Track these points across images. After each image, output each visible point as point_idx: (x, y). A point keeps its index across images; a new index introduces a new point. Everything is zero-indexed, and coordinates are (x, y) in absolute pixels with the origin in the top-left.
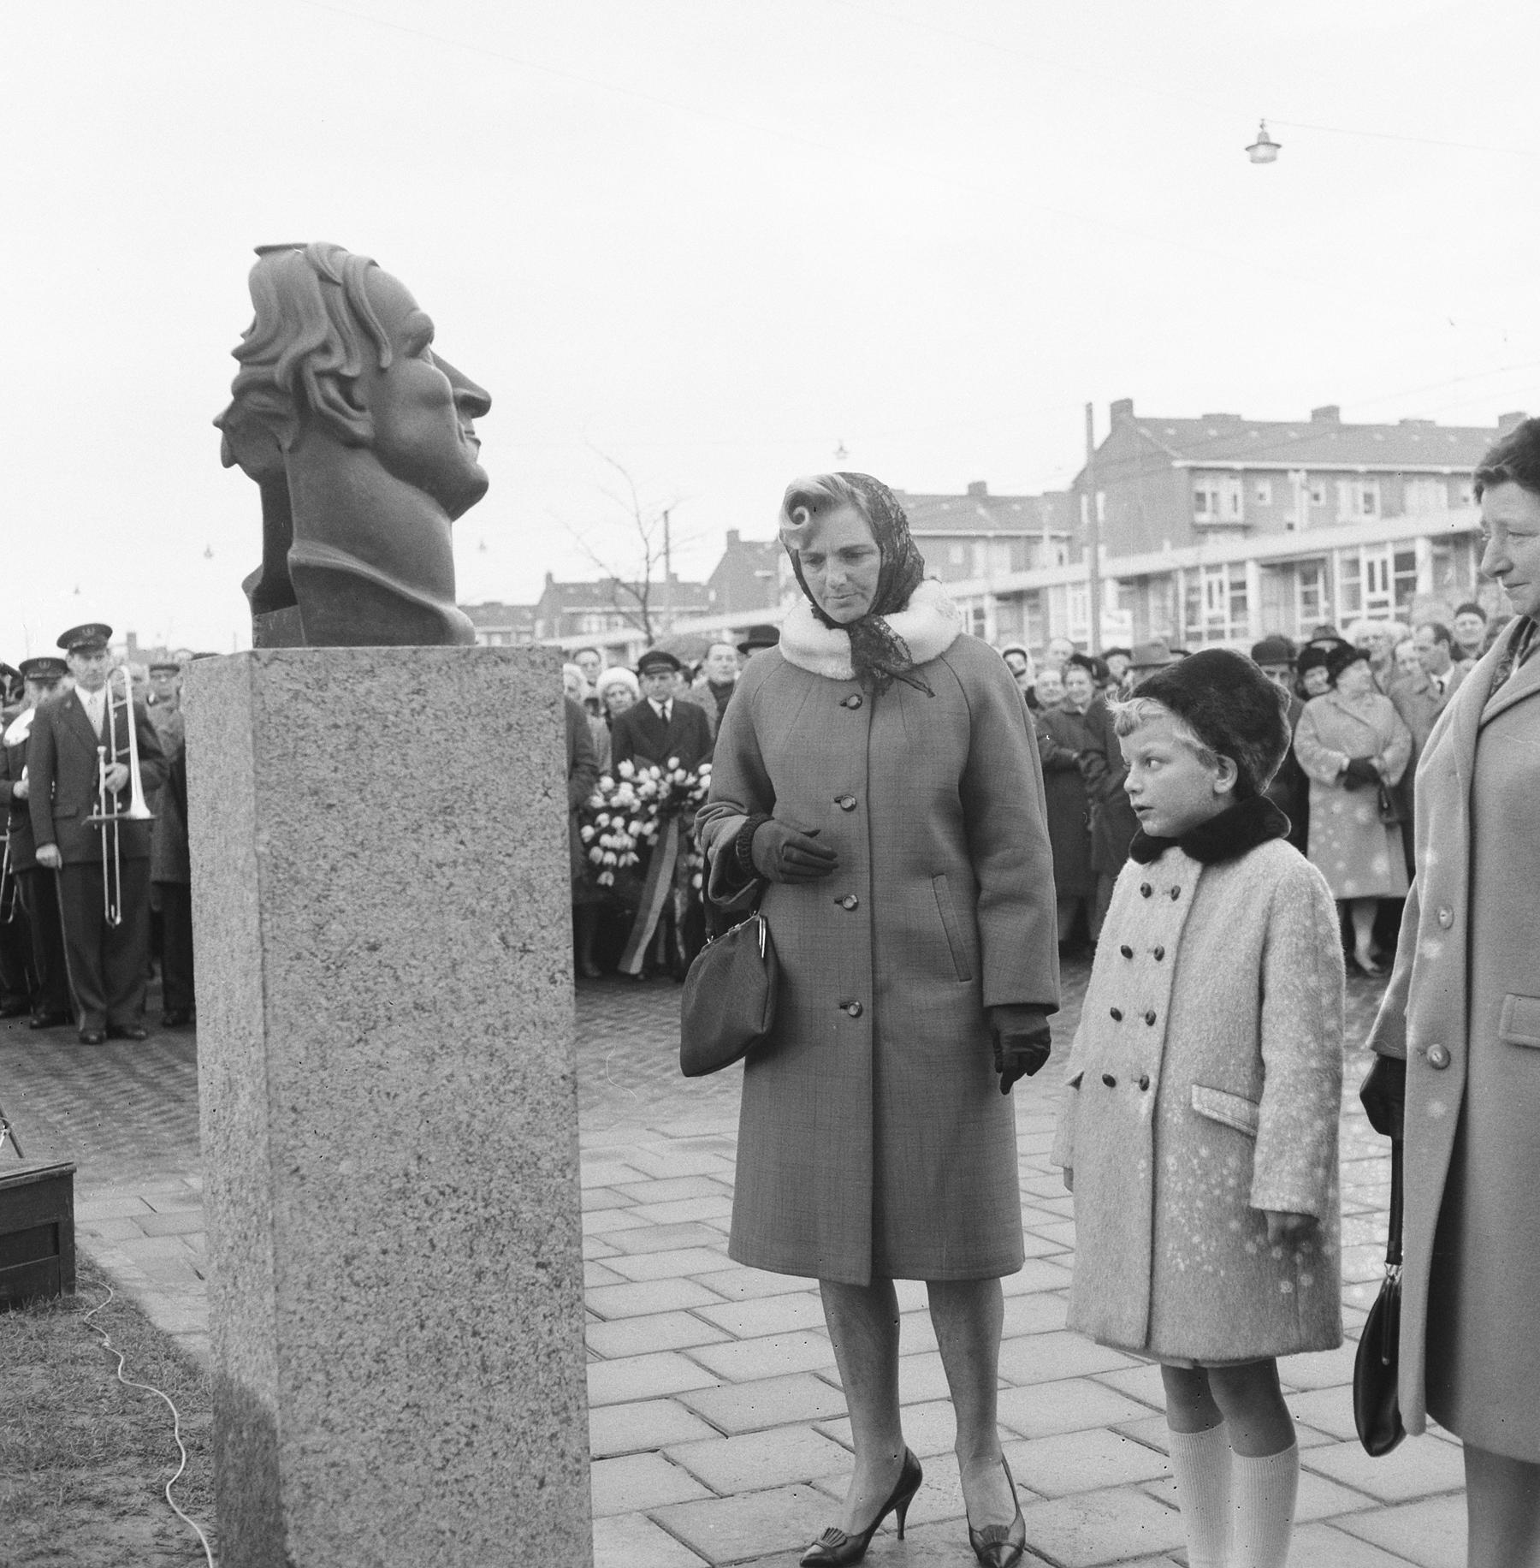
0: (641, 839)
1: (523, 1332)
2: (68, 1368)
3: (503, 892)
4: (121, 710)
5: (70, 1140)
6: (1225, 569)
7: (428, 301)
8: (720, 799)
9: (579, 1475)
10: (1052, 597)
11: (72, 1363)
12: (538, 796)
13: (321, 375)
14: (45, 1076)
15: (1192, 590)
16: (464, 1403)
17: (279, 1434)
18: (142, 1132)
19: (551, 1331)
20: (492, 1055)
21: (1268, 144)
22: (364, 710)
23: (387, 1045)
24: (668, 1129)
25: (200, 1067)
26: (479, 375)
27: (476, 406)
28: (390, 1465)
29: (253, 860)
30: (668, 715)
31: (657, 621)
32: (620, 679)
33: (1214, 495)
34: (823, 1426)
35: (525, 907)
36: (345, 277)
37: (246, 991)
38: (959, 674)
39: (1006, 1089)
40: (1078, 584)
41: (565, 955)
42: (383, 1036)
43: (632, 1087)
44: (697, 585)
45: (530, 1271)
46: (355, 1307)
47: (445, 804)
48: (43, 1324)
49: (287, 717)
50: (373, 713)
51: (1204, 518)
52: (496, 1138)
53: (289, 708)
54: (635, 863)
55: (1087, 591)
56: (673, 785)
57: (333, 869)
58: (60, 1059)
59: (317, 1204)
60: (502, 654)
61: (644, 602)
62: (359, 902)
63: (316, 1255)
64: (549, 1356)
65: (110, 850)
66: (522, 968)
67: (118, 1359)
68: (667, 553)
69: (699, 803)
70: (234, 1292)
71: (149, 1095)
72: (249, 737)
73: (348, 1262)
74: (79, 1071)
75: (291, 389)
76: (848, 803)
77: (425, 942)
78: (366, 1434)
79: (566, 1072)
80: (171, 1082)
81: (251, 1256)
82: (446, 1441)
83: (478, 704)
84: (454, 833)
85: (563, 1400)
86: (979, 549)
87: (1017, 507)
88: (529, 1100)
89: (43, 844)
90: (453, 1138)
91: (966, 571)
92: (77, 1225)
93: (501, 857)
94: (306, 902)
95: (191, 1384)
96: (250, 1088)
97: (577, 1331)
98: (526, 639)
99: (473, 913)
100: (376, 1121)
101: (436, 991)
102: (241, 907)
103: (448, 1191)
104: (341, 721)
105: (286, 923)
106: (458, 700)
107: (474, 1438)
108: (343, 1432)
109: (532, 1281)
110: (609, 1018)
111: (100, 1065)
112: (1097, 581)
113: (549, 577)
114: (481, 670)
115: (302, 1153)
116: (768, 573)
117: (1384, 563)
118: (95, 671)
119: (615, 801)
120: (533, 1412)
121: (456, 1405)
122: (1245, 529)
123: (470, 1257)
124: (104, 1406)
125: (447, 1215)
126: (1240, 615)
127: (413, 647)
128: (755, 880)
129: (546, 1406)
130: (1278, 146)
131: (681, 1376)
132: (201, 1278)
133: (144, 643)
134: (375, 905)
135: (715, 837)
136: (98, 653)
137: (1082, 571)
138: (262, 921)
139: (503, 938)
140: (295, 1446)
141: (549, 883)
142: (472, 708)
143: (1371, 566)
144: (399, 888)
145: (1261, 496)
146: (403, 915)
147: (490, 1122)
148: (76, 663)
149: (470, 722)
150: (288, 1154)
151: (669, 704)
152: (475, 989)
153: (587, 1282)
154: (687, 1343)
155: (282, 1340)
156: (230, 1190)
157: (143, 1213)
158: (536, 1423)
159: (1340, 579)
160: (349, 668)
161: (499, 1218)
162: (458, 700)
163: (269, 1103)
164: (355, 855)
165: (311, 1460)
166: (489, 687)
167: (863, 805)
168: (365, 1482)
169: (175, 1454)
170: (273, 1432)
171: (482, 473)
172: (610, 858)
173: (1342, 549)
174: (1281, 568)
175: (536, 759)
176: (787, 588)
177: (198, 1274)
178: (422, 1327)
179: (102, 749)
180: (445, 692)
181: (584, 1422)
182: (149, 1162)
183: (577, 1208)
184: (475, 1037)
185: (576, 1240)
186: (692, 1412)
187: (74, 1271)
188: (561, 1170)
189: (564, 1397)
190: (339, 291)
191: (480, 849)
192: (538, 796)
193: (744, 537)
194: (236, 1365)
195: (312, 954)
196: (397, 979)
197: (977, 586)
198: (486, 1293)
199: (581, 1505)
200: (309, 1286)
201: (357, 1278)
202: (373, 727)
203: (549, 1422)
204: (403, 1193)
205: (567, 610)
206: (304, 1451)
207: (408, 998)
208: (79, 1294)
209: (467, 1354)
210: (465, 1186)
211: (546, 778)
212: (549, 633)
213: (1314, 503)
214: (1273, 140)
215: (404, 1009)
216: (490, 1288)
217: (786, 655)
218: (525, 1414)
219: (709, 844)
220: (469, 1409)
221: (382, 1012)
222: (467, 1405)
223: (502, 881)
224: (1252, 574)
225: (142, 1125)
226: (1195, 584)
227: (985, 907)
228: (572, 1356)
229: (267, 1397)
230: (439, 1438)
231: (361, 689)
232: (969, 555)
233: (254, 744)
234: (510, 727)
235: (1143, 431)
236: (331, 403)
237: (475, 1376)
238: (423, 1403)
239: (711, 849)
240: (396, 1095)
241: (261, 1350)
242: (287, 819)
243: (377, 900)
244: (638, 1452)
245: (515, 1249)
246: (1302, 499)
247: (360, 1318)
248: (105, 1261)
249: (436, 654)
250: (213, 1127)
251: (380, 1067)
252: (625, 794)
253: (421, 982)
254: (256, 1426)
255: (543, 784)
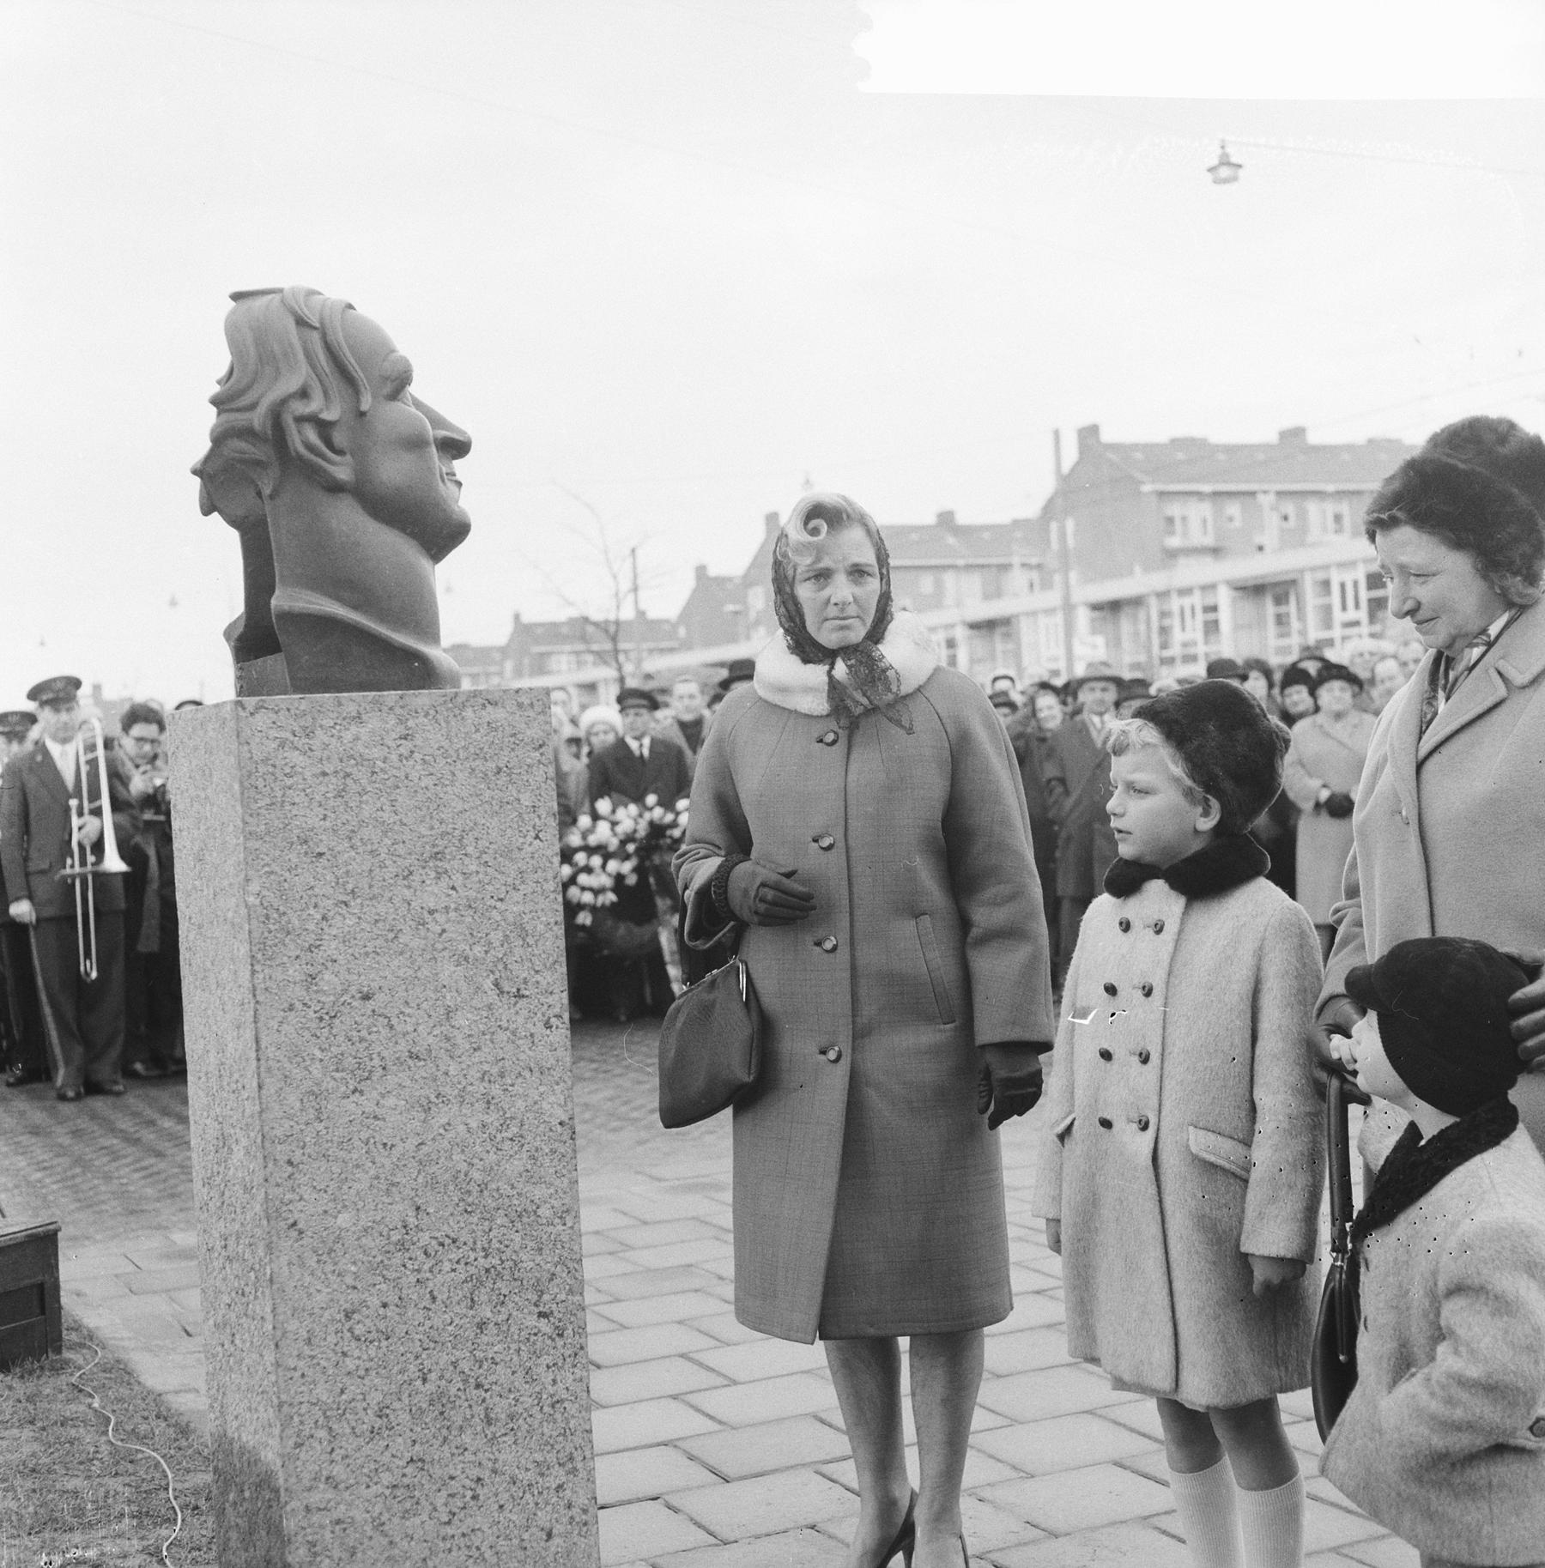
0: (619, 878)
1: (526, 1382)
2: (58, 1430)
3: (496, 937)
4: (93, 763)
5: (51, 1198)
6: (1197, 594)
7: (406, 344)
8: (697, 842)
9: (586, 1526)
10: (1024, 626)
11: (62, 1425)
12: (529, 839)
13: (300, 420)
14: (23, 1134)
15: (1164, 614)
16: (468, 1456)
17: (282, 1491)
18: (124, 1188)
19: (554, 1382)
20: (488, 1102)
21: (1229, 164)
22: (352, 757)
23: (383, 1096)
24: (655, 1171)
25: (192, 1122)
26: (461, 419)
27: (456, 447)
28: (396, 1520)
29: (243, 911)
30: (646, 752)
31: (628, 659)
32: (605, 716)
33: (1184, 519)
34: (827, 1469)
35: (518, 951)
36: (322, 323)
37: (239, 1045)
38: (938, 707)
39: (995, 1123)
40: (1050, 611)
41: (560, 999)
42: (378, 1087)
43: (614, 1130)
44: (667, 621)
45: (532, 1321)
46: (357, 1362)
47: (436, 850)
48: (30, 1386)
49: (274, 766)
50: (361, 760)
51: (1174, 542)
52: (494, 1186)
53: (276, 757)
54: (613, 904)
55: (1059, 618)
56: (652, 824)
57: (324, 918)
58: (38, 1116)
59: (315, 1259)
60: (489, 697)
61: (614, 639)
62: (350, 951)
63: (316, 1310)
64: (553, 1407)
65: (85, 904)
66: (517, 1013)
67: (108, 1420)
68: (635, 589)
69: (677, 842)
70: (232, 1349)
71: (129, 1150)
72: (237, 786)
73: (348, 1316)
74: (59, 1130)
75: (270, 432)
76: (826, 842)
77: (418, 990)
78: (370, 1490)
79: (564, 1118)
80: (152, 1136)
81: (249, 1312)
82: (452, 1496)
83: (465, 748)
84: (445, 877)
85: (568, 1450)
86: (949, 578)
87: (986, 535)
88: (526, 1147)
89: (18, 899)
90: (451, 1188)
91: (936, 601)
92: (62, 1285)
93: (492, 902)
94: (298, 953)
95: (184, 1443)
96: (244, 1142)
97: (581, 1380)
98: (495, 680)
99: (466, 959)
100: (372, 1172)
101: (431, 1040)
102: (232, 959)
103: (447, 1241)
104: (329, 768)
105: (278, 974)
106: (445, 744)
107: (479, 1491)
108: (347, 1488)
109: (536, 1331)
110: (592, 1061)
111: (79, 1121)
112: (1068, 608)
113: (517, 617)
114: (469, 713)
115: (300, 1208)
116: (738, 607)
117: (1356, 584)
118: (66, 724)
119: (593, 840)
120: (538, 1464)
121: (461, 1458)
122: (1216, 552)
123: (471, 1308)
124: (96, 1467)
125: (447, 1266)
126: (1212, 638)
127: (399, 692)
128: (732, 923)
129: (551, 1458)
130: (1240, 166)
131: (682, 1422)
132: (189, 1334)
133: (109, 694)
134: (367, 954)
135: (691, 879)
136: (68, 705)
137: (1053, 598)
138: (253, 972)
139: (497, 985)
140: (299, 1504)
141: (542, 926)
142: (461, 751)
143: (1343, 586)
144: (391, 935)
145: (1231, 519)
146: (396, 962)
147: (489, 1171)
148: (46, 716)
149: (459, 766)
150: (285, 1208)
151: (646, 741)
152: (470, 1036)
153: (589, 1329)
154: (684, 1388)
155: (284, 1397)
156: (226, 1247)
157: (127, 1271)
158: (542, 1475)
159: (1312, 599)
160: (336, 715)
161: (499, 1268)
162: (445, 744)
163: (265, 1157)
164: (346, 904)
165: (315, 1518)
166: (477, 730)
167: (841, 844)
168: (371, 1538)
169: (170, 1514)
170: (277, 1491)
171: (464, 514)
172: (587, 898)
173: (1313, 569)
174: (1255, 590)
175: (526, 799)
176: (757, 623)
177: (186, 1331)
178: (425, 1380)
179: (73, 803)
180: (431, 737)
181: (591, 1471)
182: (132, 1218)
183: (578, 1257)
184: (472, 1084)
185: (577, 1288)
186: (691, 1458)
187: (61, 1332)
188: (561, 1218)
189: (569, 1448)
190: (316, 336)
191: (472, 894)
192: (529, 839)
193: (713, 572)
194: (235, 1424)
195: (305, 1004)
196: (391, 1027)
197: (949, 615)
198: (488, 1344)
199: (589, 1556)
200: (309, 1342)
201: (357, 1332)
202: (362, 774)
203: (554, 1473)
204: (402, 1246)
205: (537, 649)
206: (308, 1509)
207: (403, 1046)
208: (67, 1354)
209: (470, 1406)
210: (464, 1236)
211: (537, 820)
212: (518, 673)
213: (1285, 525)
214: (1234, 160)
215: (398, 1059)
216: (491, 1340)
217: (761, 693)
218: (530, 1466)
219: (686, 888)
220: (473, 1462)
221: (376, 1062)
222: (473, 1458)
223: (495, 926)
224: (1224, 597)
225: (125, 1181)
226: (1166, 607)
227: (976, 944)
228: (577, 1406)
229: (270, 1456)
230: (444, 1493)
231: (348, 736)
232: (939, 585)
233: (242, 793)
234: (499, 771)
235: (1110, 455)
236: (310, 447)
237: (479, 1428)
238: (427, 1458)
239: (687, 892)
240: (393, 1146)
241: (261, 1409)
242: (277, 869)
243: (369, 949)
244: (639, 1500)
245: (517, 1299)
246: (1272, 520)
247: (362, 1373)
248: (90, 1320)
249: (422, 698)
250: (207, 1183)
251: (375, 1117)
252: (603, 833)
253: (415, 1030)
254: (258, 1486)
255: (534, 827)
